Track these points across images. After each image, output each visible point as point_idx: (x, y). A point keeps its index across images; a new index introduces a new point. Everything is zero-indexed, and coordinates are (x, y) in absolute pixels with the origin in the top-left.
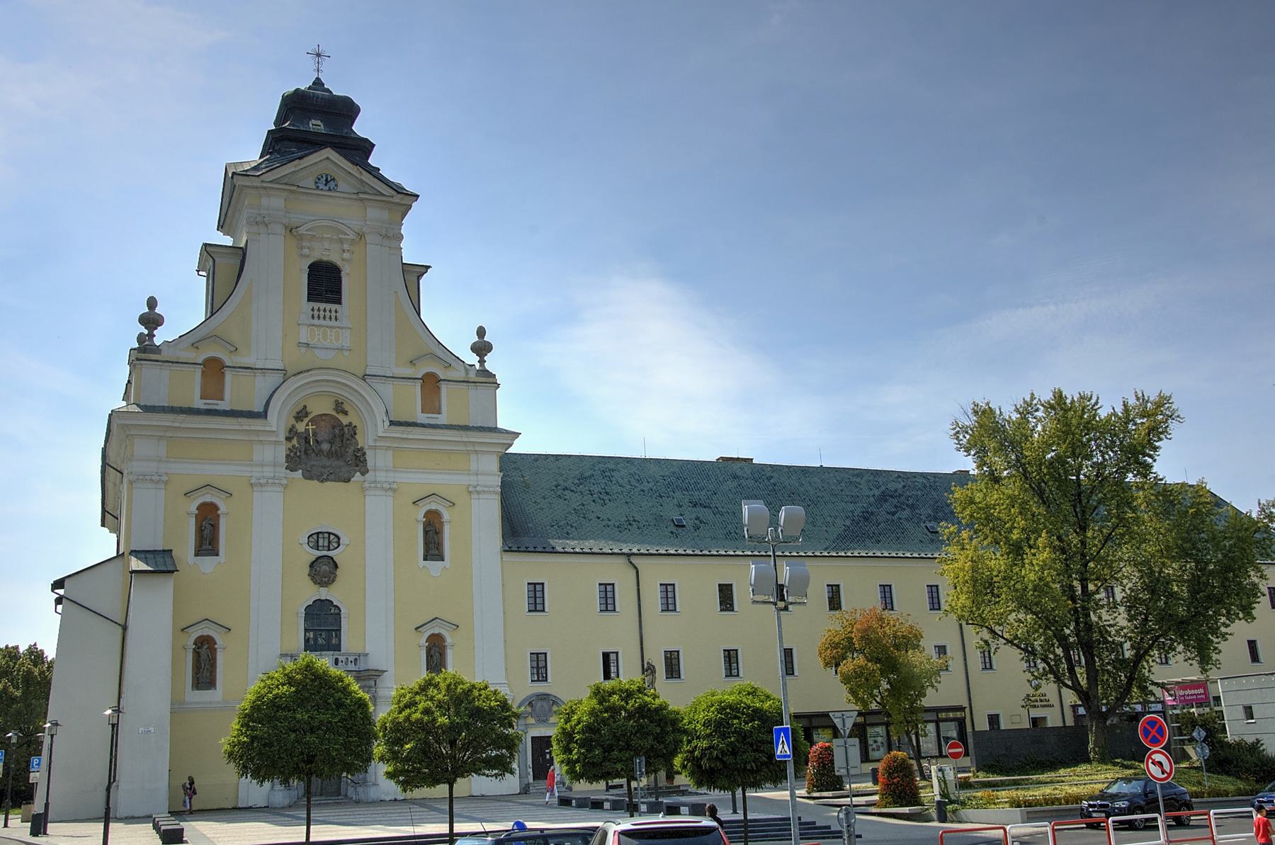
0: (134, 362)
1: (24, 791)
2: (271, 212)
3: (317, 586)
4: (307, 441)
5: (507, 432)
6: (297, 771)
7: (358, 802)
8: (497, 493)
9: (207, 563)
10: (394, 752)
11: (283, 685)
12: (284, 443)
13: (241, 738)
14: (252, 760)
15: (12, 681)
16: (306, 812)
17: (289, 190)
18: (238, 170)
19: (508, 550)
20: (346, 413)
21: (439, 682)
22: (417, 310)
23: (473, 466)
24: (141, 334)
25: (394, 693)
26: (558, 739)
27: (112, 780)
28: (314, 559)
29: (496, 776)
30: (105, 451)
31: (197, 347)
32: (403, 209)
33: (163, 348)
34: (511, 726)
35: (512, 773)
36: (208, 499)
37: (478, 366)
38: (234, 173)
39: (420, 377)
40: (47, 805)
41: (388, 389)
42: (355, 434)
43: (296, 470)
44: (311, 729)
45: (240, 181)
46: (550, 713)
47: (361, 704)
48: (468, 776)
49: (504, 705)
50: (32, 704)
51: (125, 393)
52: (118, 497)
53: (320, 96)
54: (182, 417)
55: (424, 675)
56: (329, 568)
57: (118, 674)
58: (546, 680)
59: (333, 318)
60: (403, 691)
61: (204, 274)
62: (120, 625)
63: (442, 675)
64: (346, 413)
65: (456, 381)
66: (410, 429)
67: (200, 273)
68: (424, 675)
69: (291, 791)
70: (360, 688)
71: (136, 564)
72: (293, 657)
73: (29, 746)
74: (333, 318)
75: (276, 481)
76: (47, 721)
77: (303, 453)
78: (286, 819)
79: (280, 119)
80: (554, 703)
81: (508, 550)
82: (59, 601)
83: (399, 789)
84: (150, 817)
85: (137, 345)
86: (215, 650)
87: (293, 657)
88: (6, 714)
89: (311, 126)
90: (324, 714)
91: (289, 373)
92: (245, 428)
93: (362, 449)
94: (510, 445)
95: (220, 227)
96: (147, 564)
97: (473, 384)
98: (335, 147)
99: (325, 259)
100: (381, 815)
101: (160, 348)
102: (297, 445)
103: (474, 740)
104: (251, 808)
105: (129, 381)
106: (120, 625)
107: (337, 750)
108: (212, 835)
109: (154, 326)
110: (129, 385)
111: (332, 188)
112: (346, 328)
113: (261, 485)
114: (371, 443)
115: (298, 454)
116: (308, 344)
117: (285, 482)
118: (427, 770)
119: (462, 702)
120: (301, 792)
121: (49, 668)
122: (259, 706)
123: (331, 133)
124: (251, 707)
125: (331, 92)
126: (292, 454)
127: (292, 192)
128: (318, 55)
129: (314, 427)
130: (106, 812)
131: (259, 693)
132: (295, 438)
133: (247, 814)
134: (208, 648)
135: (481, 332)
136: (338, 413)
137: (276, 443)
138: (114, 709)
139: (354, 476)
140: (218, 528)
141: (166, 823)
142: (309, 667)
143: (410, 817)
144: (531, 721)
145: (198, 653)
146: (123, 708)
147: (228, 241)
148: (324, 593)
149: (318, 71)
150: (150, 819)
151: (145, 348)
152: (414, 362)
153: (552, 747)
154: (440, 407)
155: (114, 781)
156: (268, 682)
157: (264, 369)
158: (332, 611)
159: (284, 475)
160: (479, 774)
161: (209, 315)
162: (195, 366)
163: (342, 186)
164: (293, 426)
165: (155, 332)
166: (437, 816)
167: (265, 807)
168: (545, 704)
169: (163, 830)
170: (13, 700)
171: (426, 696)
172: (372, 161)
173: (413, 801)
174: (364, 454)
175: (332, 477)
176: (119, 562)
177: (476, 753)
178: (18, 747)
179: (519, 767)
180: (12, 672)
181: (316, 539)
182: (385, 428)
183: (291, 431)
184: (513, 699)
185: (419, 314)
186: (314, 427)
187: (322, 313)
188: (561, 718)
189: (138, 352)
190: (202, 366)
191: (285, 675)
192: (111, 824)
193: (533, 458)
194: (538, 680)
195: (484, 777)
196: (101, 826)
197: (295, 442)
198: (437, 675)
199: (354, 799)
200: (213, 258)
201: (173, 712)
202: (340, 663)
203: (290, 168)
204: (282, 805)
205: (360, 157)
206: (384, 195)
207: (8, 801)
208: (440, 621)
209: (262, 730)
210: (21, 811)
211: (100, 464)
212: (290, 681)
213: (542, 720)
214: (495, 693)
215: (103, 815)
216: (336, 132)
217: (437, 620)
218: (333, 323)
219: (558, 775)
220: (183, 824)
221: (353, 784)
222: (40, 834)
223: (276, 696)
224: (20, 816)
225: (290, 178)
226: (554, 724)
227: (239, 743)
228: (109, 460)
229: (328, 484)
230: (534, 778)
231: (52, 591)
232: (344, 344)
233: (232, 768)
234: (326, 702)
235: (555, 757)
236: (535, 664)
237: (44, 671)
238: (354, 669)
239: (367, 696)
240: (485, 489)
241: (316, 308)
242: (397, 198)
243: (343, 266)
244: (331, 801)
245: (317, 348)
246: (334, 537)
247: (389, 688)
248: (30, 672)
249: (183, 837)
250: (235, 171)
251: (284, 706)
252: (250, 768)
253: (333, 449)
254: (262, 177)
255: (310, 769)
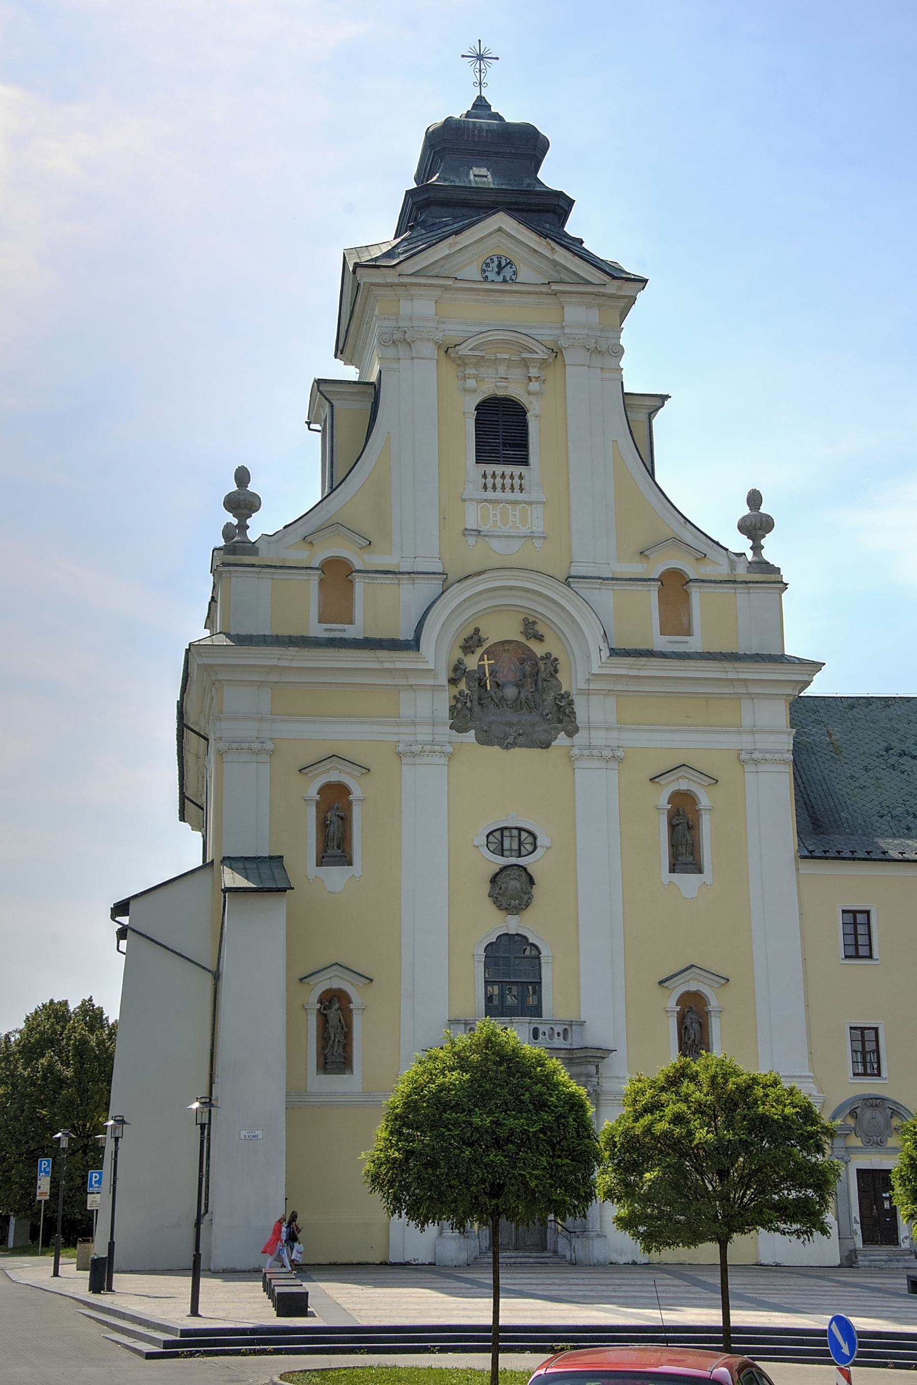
0: (219, 569)
1: (81, 1221)
2: (415, 323)
3: (503, 913)
4: (482, 684)
5: (801, 662)
6: (476, 1209)
7: (574, 1263)
8: (786, 762)
9: (335, 875)
10: (627, 1185)
11: (452, 1069)
12: (446, 688)
13: (390, 1152)
14: (407, 1187)
15: (59, 1054)
16: (492, 1276)
17: (442, 286)
18: (363, 260)
19: (808, 855)
20: (540, 638)
21: (697, 1072)
22: (651, 472)
23: (747, 719)
24: (228, 526)
25: (626, 1087)
26: (902, 1176)
27: (203, 1211)
28: (497, 870)
29: (798, 1233)
30: (182, 706)
31: (311, 543)
32: (621, 303)
33: (262, 547)
34: (819, 1149)
35: (824, 1232)
36: (334, 777)
37: (750, 555)
38: (356, 265)
39: (657, 577)
40: (111, 1245)
41: (605, 598)
42: (556, 671)
43: (465, 730)
44: (497, 1142)
45: (366, 277)
46: (889, 1130)
47: (574, 1105)
48: (750, 1231)
49: (807, 1114)
50: (88, 1090)
51: (208, 617)
52: (202, 777)
53: (485, 127)
54: (293, 651)
55: (672, 1058)
56: (521, 884)
57: (209, 1047)
58: (879, 1075)
59: (517, 487)
60: (640, 1085)
61: (318, 427)
62: (209, 971)
63: (702, 1061)
64: (540, 638)
65: (715, 582)
66: (643, 660)
67: (312, 426)
68: (672, 1058)
69: (469, 1240)
70: (571, 1077)
71: (232, 878)
72: (468, 1025)
73: (85, 1153)
74: (517, 487)
75: (437, 748)
76: (110, 1117)
77: (476, 703)
78: (463, 1285)
79: (423, 174)
80: (894, 1113)
81: (808, 855)
82: (122, 934)
83: (639, 1246)
84: (258, 1271)
85: (222, 543)
86: (351, 1011)
87: (468, 1025)
88: (53, 1103)
89: (472, 177)
90: (515, 1118)
91: (452, 577)
92: (387, 665)
93: (568, 694)
94: (807, 684)
95: (340, 351)
96: (247, 878)
97: (744, 585)
98: (510, 209)
99: (501, 393)
100: (611, 1288)
101: (256, 544)
102: (467, 691)
103: (760, 1169)
104: (408, 1264)
105: (213, 598)
106: (209, 971)
107: (537, 1177)
108: (350, 1306)
109: (246, 511)
110: (213, 604)
111: (508, 279)
112: (537, 503)
113: (413, 755)
114: (582, 685)
115: (469, 704)
116: (479, 531)
117: (449, 749)
118: (682, 1217)
119: (737, 1106)
120: (486, 1242)
121: (110, 1035)
122: (416, 1102)
123: (504, 187)
124: (405, 1104)
125: (501, 119)
126: (459, 705)
127: (446, 288)
128: (480, 57)
129: (493, 662)
130: (195, 1260)
131: (416, 1081)
132: (464, 679)
133: (403, 1275)
134: (340, 1008)
135: (754, 499)
136: (528, 638)
137: (435, 688)
138: (203, 1100)
139: (555, 738)
140: (351, 821)
141: (282, 1282)
142: (489, 1042)
143: (655, 1295)
144: (855, 1141)
145: (325, 1015)
146: (217, 1100)
147: (351, 373)
148: (513, 925)
149: (480, 84)
150: (257, 1275)
151: (235, 547)
152: (647, 553)
153: (893, 1190)
154: (690, 624)
155: (206, 1211)
156: (430, 1065)
157: (413, 573)
158: (527, 953)
159: (447, 739)
160: (770, 1229)
161: (327, 490)
162: (309, 571)
163: (526, 274)
164: (460, 662)
165: (248, 521)
166: (704, 1296)
167: (430, 1264)
168: (879, 1117)
169: (278, 1293)
170: (61, 1082)
171: (677, 1093)
172: (571, 228)
173: (662, 1267)
174: (571, 703)
175: (521, 740)
176: (205, 876)
177: (763, 1192)
178: (71, 1154)
179: (837, 1219)
180: (59, 1040)
181: (499, 838)
182: (603, 660)
183: (456, 669)
184: (823, 1104)
185: (652, 475)
186: (493, 662)
187: (499, 481)
188: (906, 1140)
189: (225, 554)
190: (320, 572)
191: (455, 1054)
192: (201, 1279)
193: (845, 704)
194: (865, 1074)
195: (778, 1234)
196: (188, 1281)
197: (463, 685)
198: (694, 1060)
199: (568, 1257)
200: (330, 402)
201: (290, 1107)
202: (541, 1036)
203: (443, 249)
204: (456, 1263)
205: (550, 224)
206: (591, 283)
207: (59, 1237)
208: (698, 971)
209: (424, 1140)
210: (77, 1251)
211: (175, 726)
212: (462, 1064)
213: (875, 1142)
214: (791, 1092)
215: (191, 1265)
216: (511, 185)
217: (694, 969)
218: (517, 496)
219: (906, 1238)
220: (307, 1286)
221: (565, 1233)
222: (103, 1290)
223: (442, 1088)
224: (75, 1260)
225: (442, 266)
226: (895, 1150)
227: (387, 1160)
228: (188, 719)
229: (516, 751)
230: (864, 1242)
231: (113, 918)
232: (534, 529)
233: (377, 1201)
234: (518, 1099)
235: (899, 1207)
236: (859, 1047)
237: (104, 1040)
238: (563, 1046)
239: (582, 1091)
240: (768, 756)
241: (489, 474)
242: (613, 287)
243: (531, 403)
244: (531, 1260)
245: (493, 536)
246: (527, 835)
247: (618, 1078)
248: (84, 1041)
249: (307, 1307)
250: (358, 261)
251: (453, 1103)
252: (405, 1202)
253: (522, 696)
254: (399, 268)
255: (497, 1206)
